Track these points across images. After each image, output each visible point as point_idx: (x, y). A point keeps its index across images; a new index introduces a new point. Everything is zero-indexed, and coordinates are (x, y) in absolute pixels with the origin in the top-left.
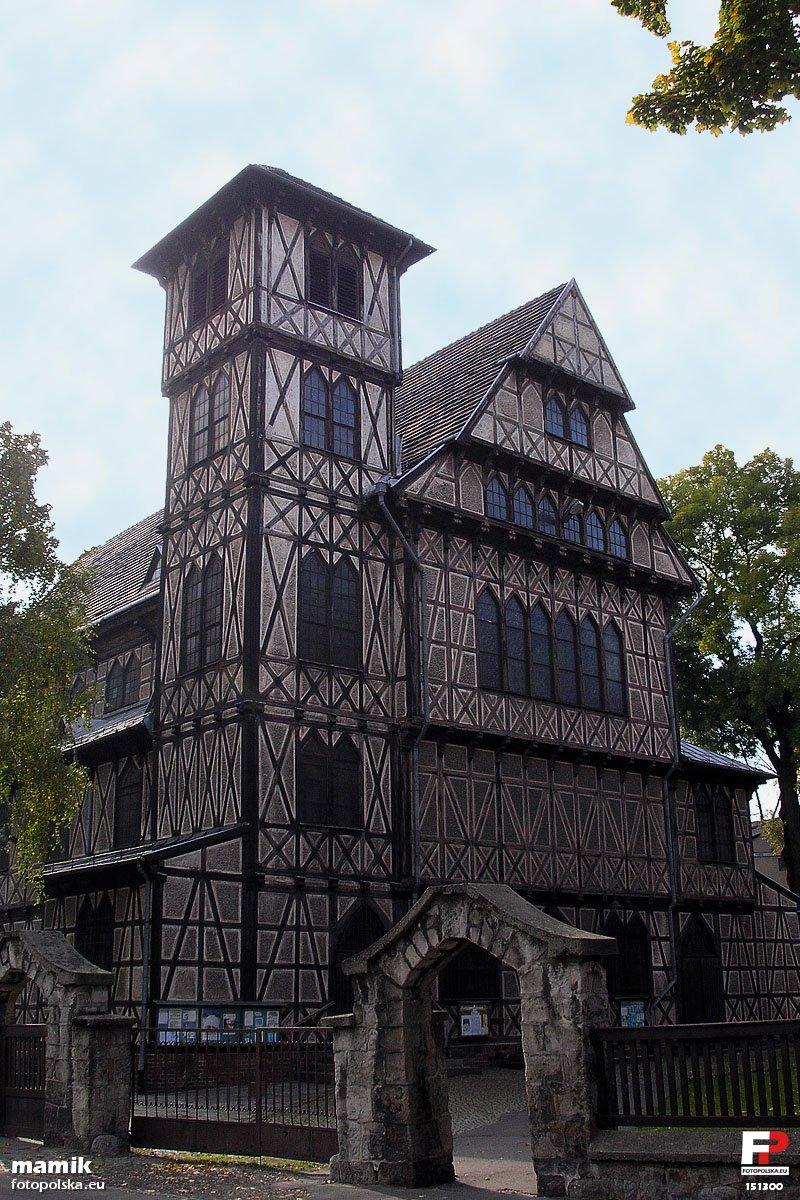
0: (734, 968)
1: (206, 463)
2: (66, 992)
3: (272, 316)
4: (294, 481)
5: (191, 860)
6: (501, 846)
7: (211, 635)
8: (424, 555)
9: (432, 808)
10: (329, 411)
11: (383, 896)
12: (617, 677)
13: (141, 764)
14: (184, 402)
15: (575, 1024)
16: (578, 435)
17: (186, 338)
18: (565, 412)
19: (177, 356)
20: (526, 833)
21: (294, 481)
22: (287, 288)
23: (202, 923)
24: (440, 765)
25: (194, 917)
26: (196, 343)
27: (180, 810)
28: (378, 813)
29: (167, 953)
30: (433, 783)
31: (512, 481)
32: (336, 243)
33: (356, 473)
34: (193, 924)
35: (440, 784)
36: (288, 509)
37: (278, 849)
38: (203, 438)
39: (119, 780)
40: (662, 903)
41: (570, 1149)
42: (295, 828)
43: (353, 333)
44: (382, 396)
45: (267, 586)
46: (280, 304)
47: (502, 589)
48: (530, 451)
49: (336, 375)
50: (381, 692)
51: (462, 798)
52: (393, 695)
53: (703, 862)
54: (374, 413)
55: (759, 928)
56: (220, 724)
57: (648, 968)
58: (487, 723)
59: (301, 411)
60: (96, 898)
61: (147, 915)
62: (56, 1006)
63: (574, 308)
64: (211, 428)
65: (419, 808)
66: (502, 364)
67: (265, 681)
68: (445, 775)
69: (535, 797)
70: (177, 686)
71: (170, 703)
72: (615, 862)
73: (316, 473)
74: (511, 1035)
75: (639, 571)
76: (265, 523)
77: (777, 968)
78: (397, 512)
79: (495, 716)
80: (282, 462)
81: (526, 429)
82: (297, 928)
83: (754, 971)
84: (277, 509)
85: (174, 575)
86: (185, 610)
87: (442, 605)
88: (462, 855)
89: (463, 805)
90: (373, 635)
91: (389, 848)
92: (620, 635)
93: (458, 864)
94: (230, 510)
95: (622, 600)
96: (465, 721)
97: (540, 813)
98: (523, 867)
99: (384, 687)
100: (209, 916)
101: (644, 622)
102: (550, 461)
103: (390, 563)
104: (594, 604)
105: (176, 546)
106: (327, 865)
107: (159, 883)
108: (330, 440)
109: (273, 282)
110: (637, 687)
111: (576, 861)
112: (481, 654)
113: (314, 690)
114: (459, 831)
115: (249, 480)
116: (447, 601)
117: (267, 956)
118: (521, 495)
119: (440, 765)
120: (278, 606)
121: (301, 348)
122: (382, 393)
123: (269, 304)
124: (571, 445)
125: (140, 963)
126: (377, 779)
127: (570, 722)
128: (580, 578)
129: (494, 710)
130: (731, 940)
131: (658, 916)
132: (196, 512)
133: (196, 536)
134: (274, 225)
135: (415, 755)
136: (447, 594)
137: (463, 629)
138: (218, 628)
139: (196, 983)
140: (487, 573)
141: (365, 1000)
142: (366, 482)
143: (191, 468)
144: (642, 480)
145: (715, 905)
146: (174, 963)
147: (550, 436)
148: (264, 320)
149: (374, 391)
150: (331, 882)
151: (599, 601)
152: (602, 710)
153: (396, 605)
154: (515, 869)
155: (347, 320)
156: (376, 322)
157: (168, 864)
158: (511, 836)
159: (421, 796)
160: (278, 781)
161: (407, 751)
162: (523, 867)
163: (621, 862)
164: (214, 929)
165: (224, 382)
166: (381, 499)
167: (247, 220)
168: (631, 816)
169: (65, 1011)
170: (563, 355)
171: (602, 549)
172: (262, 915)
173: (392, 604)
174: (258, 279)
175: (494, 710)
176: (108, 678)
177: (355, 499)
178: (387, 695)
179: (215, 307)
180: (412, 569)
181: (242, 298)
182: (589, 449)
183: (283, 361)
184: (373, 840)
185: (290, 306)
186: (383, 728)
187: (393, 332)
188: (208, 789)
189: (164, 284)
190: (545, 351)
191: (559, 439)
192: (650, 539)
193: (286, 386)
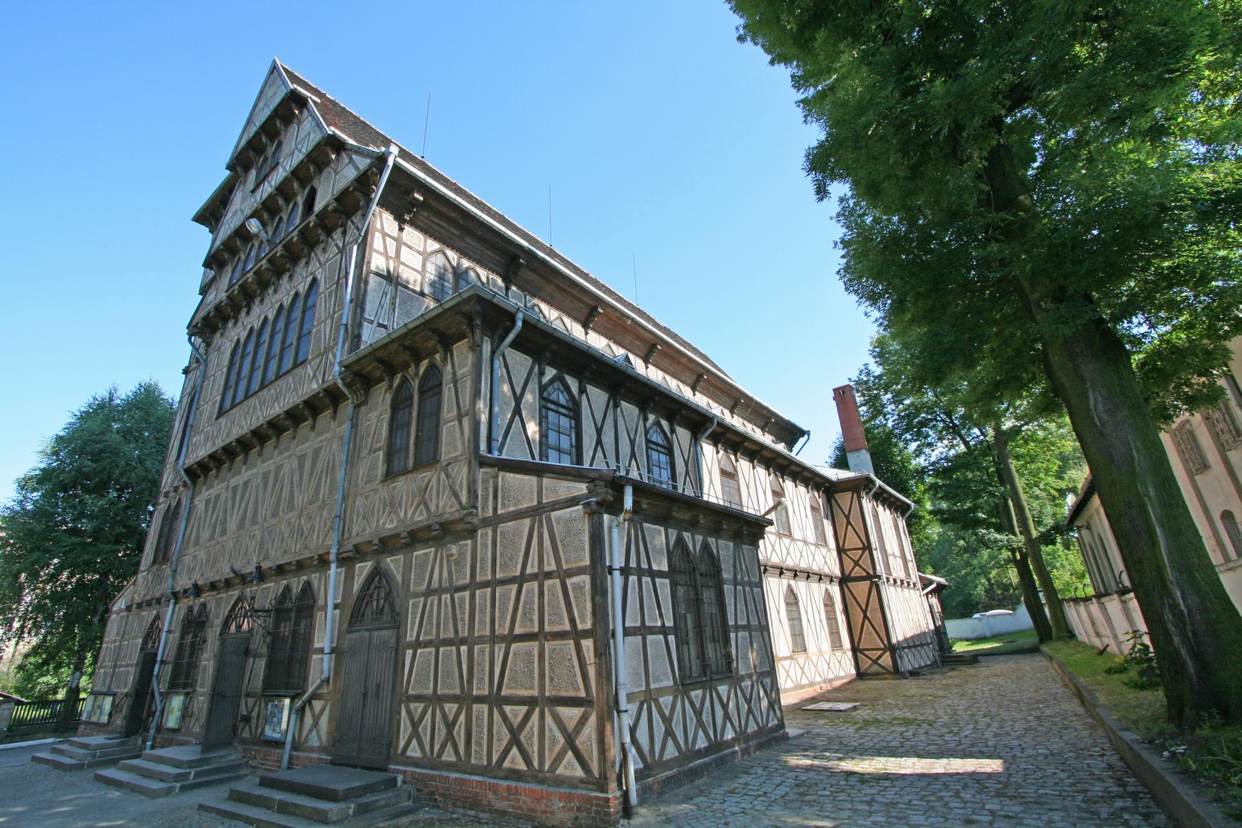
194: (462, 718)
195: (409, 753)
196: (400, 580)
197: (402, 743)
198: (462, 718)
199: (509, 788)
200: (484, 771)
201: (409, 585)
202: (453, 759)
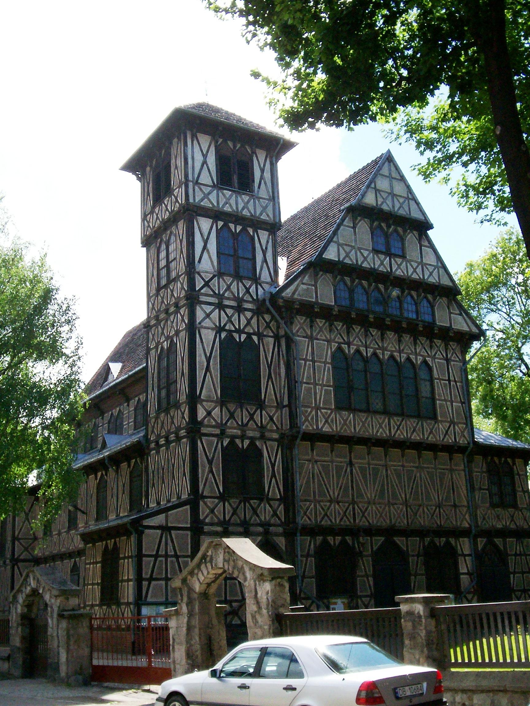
0: (519, 573)
1: (166, 286)
2: (56, 599)
3: (197, 197)
4: (215, 295)
5: (159, 520)
6: (353, 502)
7: (172, 388)
8: (298, 331)
9: (308, 482)
10: (235, 250)
11: (277, 535)
12: (429, 395)
13: (141, 463)
14: (153, 250)
15: (268, 612)
16: (395, 249)
17: (152, 212)
18: (387, 236)
19: (148, 222)
20: (370, 493)
21: (215, 295)
22: (205, 179)
23: (166, 556)
24: (312, 455)
25: (162, 552)
26: (157, 215)
27: (160, 489)
28: (274, 487)
29: (146, 574)
30: (308, 466)
31: (353, 281)
32: (235, 146)
33: (254, 286)
34: (161, 556)
35: (313, 468)
36: (211, 312)
37: (212, 511)
38: (164, 272)
39: (131, 473)
40: (465, 533)
42: (222, 498)
43: (248, 201)
44: (269, 238)
45: (201, 359)
46: (201, 189)
47: (349, 347)
48: (363, 262)
49: (239, 228)
50: (274, 415)
51: (328, 474)
52: (281, 416)
53: (493, 506)
54: (264, 248)
56: (178, 439)
57: (457, 574)
58: (341, 428)
59: (218, 253)
60: (111, 543)
61: (135, 553)
62: (52, 607)
63: (390, 170)
64: (168, 266)
65: (300, 482)
66: (343, 210)
67: (201, 413)
69: (376, 472)
70: (157, 418)
71: (153, 427)
72: (432, 509)
73: (228, 288)
75: (441, 328)
76: (198, 321)
78: (278, 309)
79: (346, 424)
80: (207, 284)
81: (360, 249)
84: (205, 312)
85: (153, 352)
86: (159, 373)
87: (310, 361)
88: (328, 509)
89: (328, 478)
90: (268, 382)
91: (282, 507)
92: (430, 369)
93: (326, 515)
94: (179, 315)
95: (431, 347)
96: (326, 429)
97: (380, 481)
98: (369, 514)
99: (276, 412)
100: (171, 552)
101: (448, 360)
102: (376, 267)
103: (277, 338)
104: (411, 350)
105: (153, 335)
107: (140, 534)
108: (237, 268)
109: (196, 176)
110: (442, 400)
111: (405, 509)
112: (336, 388)
113: (232, 416)
114: (325, 495)
115: (187, 297)
116: (313, 358)
118: (359, 290)
119: (312, 455)
120: (208, 369)
122: (269, 236)
123: (194, 190)
125: (131, 580)
126: (273, 465)
127: (396, 425)
128: (402, 336)
129: (345, 421)
131: (463, 541)
132: (172, 309)
133: (163, 329)
134: (195, 142)
135: (296, 451)
136: (313, 353)
137: (324, 374)
138: (145, 394)
139: (164, 590)
140: (339, 338)
141: (182, 600)
142: (260, 291)
143: (159, 289)
144: (440, 272)
145: (503, 533)
146: (151, 579)
147: (376, 251)
148: (191, 200)
149: (264, 235)
150: (245, 528)
151: (415, 349)
152: (419, 416)
153: (282, 362)
156: (263, 193)
157: (146, 523)
158: (360, 495)
159: (300, 476)
160: (211, 471)
162: (369, 514)
163: (436, 509)
165: (173, 238)
166: (267, 303)
167: (179, 139)
169: (56, 609)
170: (382, 200)
173: (279, 361)
174: (186, 176)
175: (345, 421)
176: (135, 410)
177: (254, 301)
178: (278, 417)
179: (165, 193)
180: (289, 341)
181: (179, 187)
182: (403, 257)
183: (205, 224)
184: (272, 502)
185: (207, 190)
186: (275, 436)
187: (274, 198)
188: (173, 477)
189: (139, 179)
190: (370, 199)
191: (382, 253)
192: (448, 309)
193: (208, 238)
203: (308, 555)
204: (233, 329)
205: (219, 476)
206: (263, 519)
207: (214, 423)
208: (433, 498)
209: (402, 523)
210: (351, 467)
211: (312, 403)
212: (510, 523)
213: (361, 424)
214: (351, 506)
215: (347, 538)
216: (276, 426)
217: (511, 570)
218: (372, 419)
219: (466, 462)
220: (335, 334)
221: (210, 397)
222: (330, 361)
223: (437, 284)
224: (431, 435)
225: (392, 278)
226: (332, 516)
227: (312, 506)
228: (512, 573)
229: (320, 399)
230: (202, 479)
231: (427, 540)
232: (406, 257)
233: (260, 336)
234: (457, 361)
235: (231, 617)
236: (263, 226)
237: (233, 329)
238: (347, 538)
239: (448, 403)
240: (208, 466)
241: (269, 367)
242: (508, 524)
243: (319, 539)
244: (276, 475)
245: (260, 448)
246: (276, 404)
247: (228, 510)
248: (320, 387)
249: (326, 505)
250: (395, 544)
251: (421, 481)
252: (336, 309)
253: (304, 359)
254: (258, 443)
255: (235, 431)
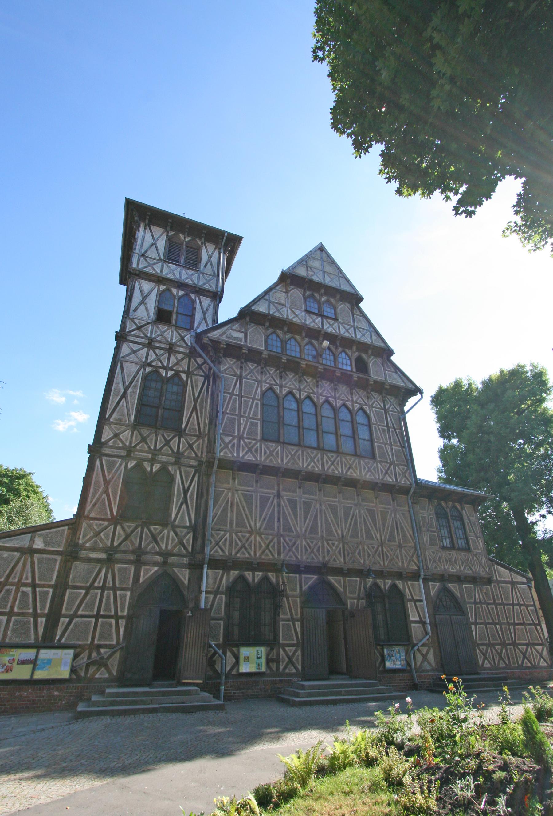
0: (481, 624)
11: (181, 566)
22: (152, 253)
30: (227, 494)
41: (457, 758)
51: (250, 504)
55: (497, 595)
68: (237, 490)
69: (307, 505)
74: (287, 671)
76: (122, 355)
77: (518, 624)
82: (103, 588)
83: (498, 626)
93: (243, 546)
106: (137, 544)
114: (245, 525)
117: (71, 609)
120: (124, 395)
121: (159, 280)
124: (323, 316)
126: (186, 492)
130: (475, 603)
145: (459, 579)
151: (352, 398)
154: (312, 551)
155: (189, 269)
160: (106, 492)
161: (209, 475)
164: (518, 607)
168: (384, 519)
171: (332, 364)
172: (74, 578)
178: (199, 444)
194: (504, 651)
195: (485, 666)
196: (459, 595)
197: (480, 663)
198: (504, 651)
199: (529, 672)
200: (517, 668)
201: (15, 590)
202: (504, 665)
203: (216, 592)
204: (161, 366)
205: (115, 498)
206: (163, 547)
207: (121, 445)
208: (374, 536)
209: (340, 562)
210: (343, 536)
211: (234, 433)
212: (464, 568)
213: (290, 456)
214: (276, 539)
215: (270, 574)
216: (195, 453)
217: (472, 620)
218: (302, 452)
219: (410, 502)
220: (266, 377)
221: (120, 420)
222: (259, 398)
223: (369, 343)
224: (369, 474)
225: (323, 332)
226: (251, 548)
227: (228, 535)
228: (472, 623)
229: (245, 429)
230: (92, 499)
231: (370, 581)
232: (338, 320)
233: (188, 373)
234: (395, 412)
235: (95, 668)
236: (206, 293)
237: (161, 366)
238: (270, 574)
239: (387, 446)
240: (103, 486)
241: (196, 401)
242: (462, 568)
243: (234, 574)
244: (189, 501)
245: (173, 472)
246: (198, 433)
247: (119, 534)
248: (245, 419)
249: (244, 537)
250: (330, 584)
251: (360, 518)
252: (266, 353)
253: (230, 393)
254: (170, 468)
255: (145, 454)
